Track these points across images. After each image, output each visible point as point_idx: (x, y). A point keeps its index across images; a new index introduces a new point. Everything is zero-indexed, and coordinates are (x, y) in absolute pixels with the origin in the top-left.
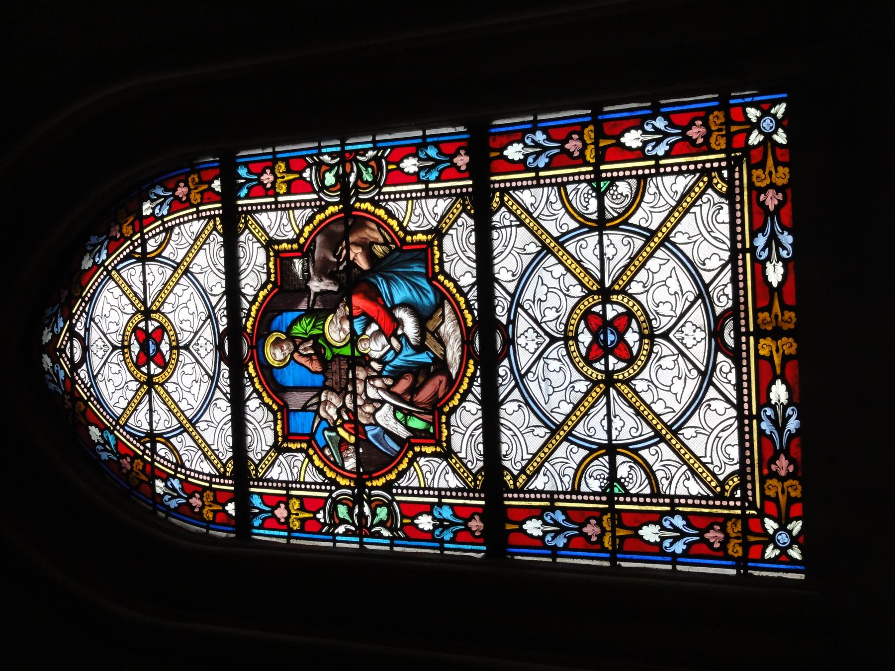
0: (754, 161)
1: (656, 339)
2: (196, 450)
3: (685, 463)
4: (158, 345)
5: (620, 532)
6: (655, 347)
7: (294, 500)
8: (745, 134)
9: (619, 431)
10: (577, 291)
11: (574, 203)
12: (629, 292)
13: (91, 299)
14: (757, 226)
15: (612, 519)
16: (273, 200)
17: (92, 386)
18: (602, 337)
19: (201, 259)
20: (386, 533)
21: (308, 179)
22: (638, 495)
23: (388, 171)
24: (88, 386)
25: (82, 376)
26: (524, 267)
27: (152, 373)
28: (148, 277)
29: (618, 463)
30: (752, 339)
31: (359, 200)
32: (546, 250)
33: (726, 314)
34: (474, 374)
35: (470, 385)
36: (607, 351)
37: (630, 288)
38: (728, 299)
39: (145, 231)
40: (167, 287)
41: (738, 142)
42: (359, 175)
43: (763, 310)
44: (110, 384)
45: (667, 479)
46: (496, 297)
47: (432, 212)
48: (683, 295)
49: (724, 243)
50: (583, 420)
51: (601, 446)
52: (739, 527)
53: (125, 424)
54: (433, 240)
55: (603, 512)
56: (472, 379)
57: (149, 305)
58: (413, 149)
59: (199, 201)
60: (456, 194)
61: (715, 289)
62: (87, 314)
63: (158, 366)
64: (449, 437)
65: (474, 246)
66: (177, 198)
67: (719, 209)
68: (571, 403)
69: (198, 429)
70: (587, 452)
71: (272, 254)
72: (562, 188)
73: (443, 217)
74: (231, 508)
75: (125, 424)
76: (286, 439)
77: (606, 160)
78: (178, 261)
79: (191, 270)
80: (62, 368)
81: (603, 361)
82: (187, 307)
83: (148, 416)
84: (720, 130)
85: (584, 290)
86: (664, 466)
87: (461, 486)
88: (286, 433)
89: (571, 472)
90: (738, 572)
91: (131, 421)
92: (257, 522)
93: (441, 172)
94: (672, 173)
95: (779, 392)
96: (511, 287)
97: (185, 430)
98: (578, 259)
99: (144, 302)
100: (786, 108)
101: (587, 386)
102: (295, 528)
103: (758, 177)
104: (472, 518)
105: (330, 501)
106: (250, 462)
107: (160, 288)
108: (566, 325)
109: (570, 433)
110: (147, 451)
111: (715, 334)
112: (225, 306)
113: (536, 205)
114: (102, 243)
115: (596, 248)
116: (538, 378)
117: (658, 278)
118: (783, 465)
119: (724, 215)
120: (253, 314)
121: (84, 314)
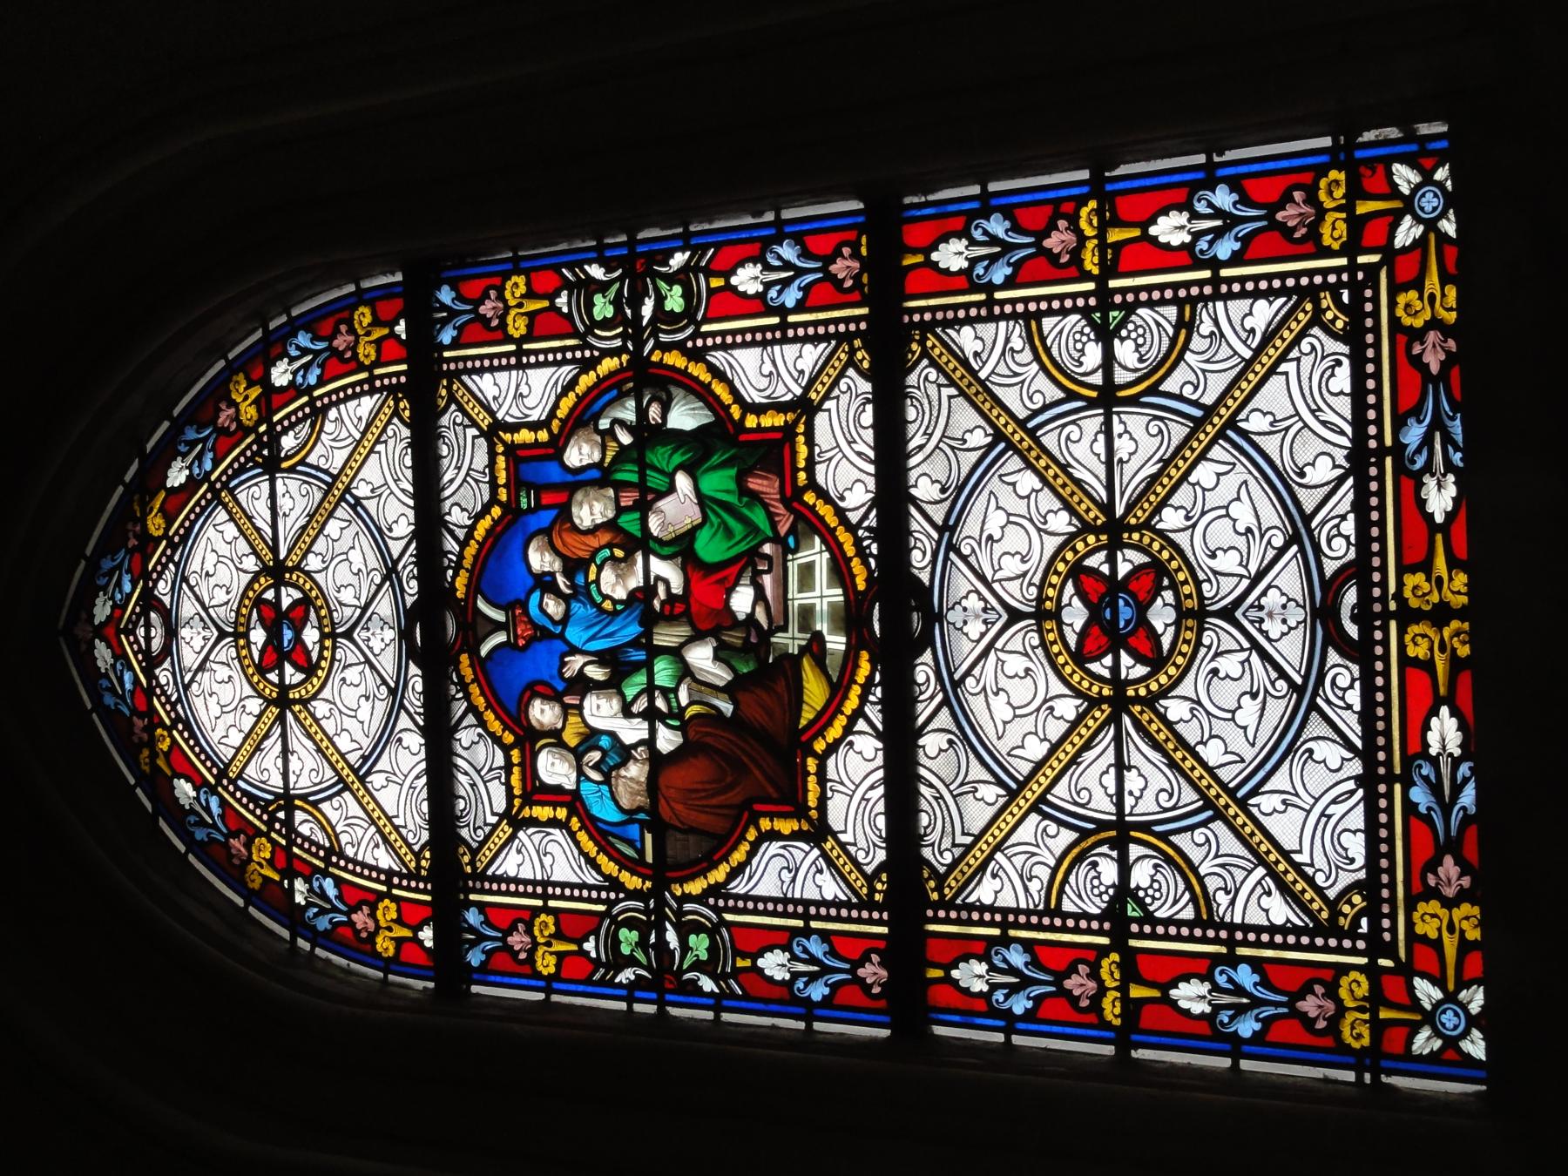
0: (1402, 277)
1: (1208, 620)
2: (366, 825)
4: (1142, 608)
5: (1136, 992)
6: (1206, 633)
8: (1390, 219)
9: (1137, 799)
10: (1175, 709)
11: (1055, 352)
13: (184, 539)
14: (1406, 404)
17: (179, 700)
18: (1108, 614)
19: (372, 472)
20: (707, 984)
21: (565, 310)
22: (1167, 922)
23: (710, 291)
24: (173, 699)
25: (163, 681)
26: (963, 475)
27: (287, 682)
28: (280, 501)
29: (1132, 858)
30: (1393, 625)
31: (660, 346)
33: (1344, 574)
34: (870, 678)
35: (863, 699)
38: (1349, 543)
39: (276, 418)
40: (316, 520)
41: (1372, 235)
42: (660, 300)
43: (1413, 570)
44: (212, 701)
45: (1228, 893)
48: (984, 689)
49: (1342, 433)
50: (1069, 773)
51: (1102, 825)
52: (1363, 989)
53: (239, 776)
55: (1103, 951)
56: (458, 567)
58: (755, 249)
59: (523, 331)
60: (837, 335)
61: (1323, 523)
62: (177, 565)
63: (298, 668)
64: (823, 800)
65: (871, 431)
67: (1333, 367)
69: (369, 786)
71: (500, 449)
73: (812, 382)
74: (427, 935)
75: (239, 776)
77: (1121, 269)
79: (354, 491)
80: (131, 668)
83: (280, 762)
85: (1162, 710)
86: (1222, 866)
88: (529, 789)
89: (1044, 873)
90: (1360, 1077)
91: (251, 771)
94: (1243, 294)
95: (1445, 732)
96: (938, 514)
97: (347, 788)
98: (1063, 462)
99: (274, 549)
103: (1408, 306)
104: (864, 959)
107: (302, 522)
108: (1041, 588)
109: (1042, 799)
110: (277, 826)
111: (1323, 613)
113: (1259, 890)
114: (119, 566)
117: (1213, 499)
119: (1342, 379)
120: (467, 563)
121: (171, 566)
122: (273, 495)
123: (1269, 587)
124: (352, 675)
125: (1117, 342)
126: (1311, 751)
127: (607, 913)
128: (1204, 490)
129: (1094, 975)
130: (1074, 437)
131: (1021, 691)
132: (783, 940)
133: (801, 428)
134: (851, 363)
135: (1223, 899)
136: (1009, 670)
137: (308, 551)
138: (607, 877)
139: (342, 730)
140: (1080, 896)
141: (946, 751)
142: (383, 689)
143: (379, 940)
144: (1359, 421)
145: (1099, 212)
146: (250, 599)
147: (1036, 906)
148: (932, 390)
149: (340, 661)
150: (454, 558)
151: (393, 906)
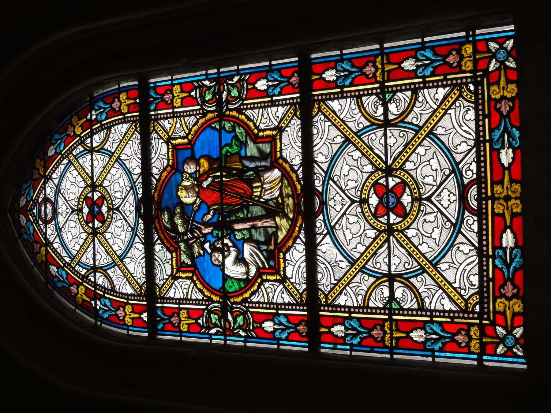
1: (423, 201)
2: (123, 278)
3: (440, 287)
4: (100, 207)
7: (183, 311)
8: (488, 59)
9: (397, 266)
10: (369, 168)
12: (405, 169)
15: (391, 325)
16: (171, 111)
19: (127, 150)
20: (243, 333)
22: (408, 309)
23: (248, 89)
27: (96, 227)
28: (94, 162)
30: (490, 202)
32: (347, 141)
36: (388, 210)
37: (375, 233)
38: (473, 173)
39: (94, 128)
40: (106, 170)
41: (481, 65)
42: (229, 92)
46: (315, 174)
47: (274, 115)
49: (470, 134)
51: (384, 275)
54: (276, 135)
55: (385, 320)
57: (95, 180)
60: (290, 104)
61: (464, 166)
63: (100, 222)
66: (113, 109)
67: (467, 111)
68: (364, 245)
69: (124, 263)
70: (406, 120)
72: (359, 100)
74: (145, 316)
76: (178, 271)
78: (113, 151)
79: (121, 157)
81: (386, 217)
82: (118, 182)
84: (470, 57)
87: (134, 293)
92: (160, 326)
93: (282, 88)
94: (433, 87)
95: (508, 240)
99: (92, 178)
100: (513, 42)
101: (405, 167)
102: (184, 330)
104: (299, 324)
105: (206, 311)
106: (320, 293)
107: (101, 170)
112: (141, 181)
113: (341, 111)
115: (381, 138)
116: (342, 227)
118: (509, 289)
122: (92, 159)
123: (444, 188)
124: (119, 223)
125: (389, 104)
126: (459, 247)
127: (243, 100)
128: (421, 156)
129: (382, 329)
130: (374, 138)
131: (355, 228)
132: (271, 317)
133: (278, 137)
134: (295, 115)
135: (427, 301)
136: (351, 222)
137: (104, 179)
138: (207, 297)
139: (115, 243)
140: (376, 300)
141: (458, 145)
142: (130, 228)
143: (126, 319)
144: (477, 132)
145: (382, 59)
146: (83, 196)
147: (360, 305)
148: (323, 123)
149: (115, 218)
150: (154, 186)
151: (130, 306)
